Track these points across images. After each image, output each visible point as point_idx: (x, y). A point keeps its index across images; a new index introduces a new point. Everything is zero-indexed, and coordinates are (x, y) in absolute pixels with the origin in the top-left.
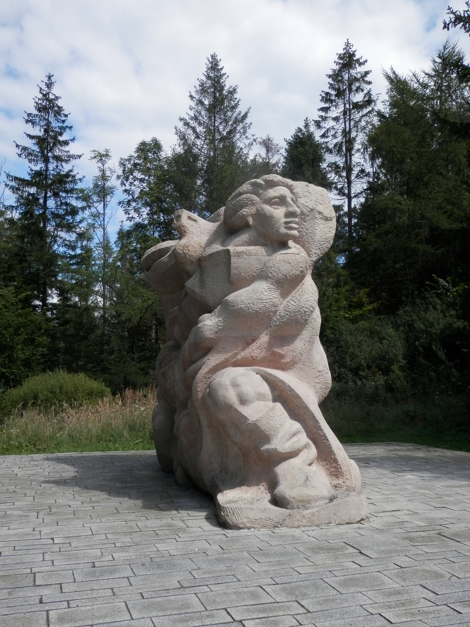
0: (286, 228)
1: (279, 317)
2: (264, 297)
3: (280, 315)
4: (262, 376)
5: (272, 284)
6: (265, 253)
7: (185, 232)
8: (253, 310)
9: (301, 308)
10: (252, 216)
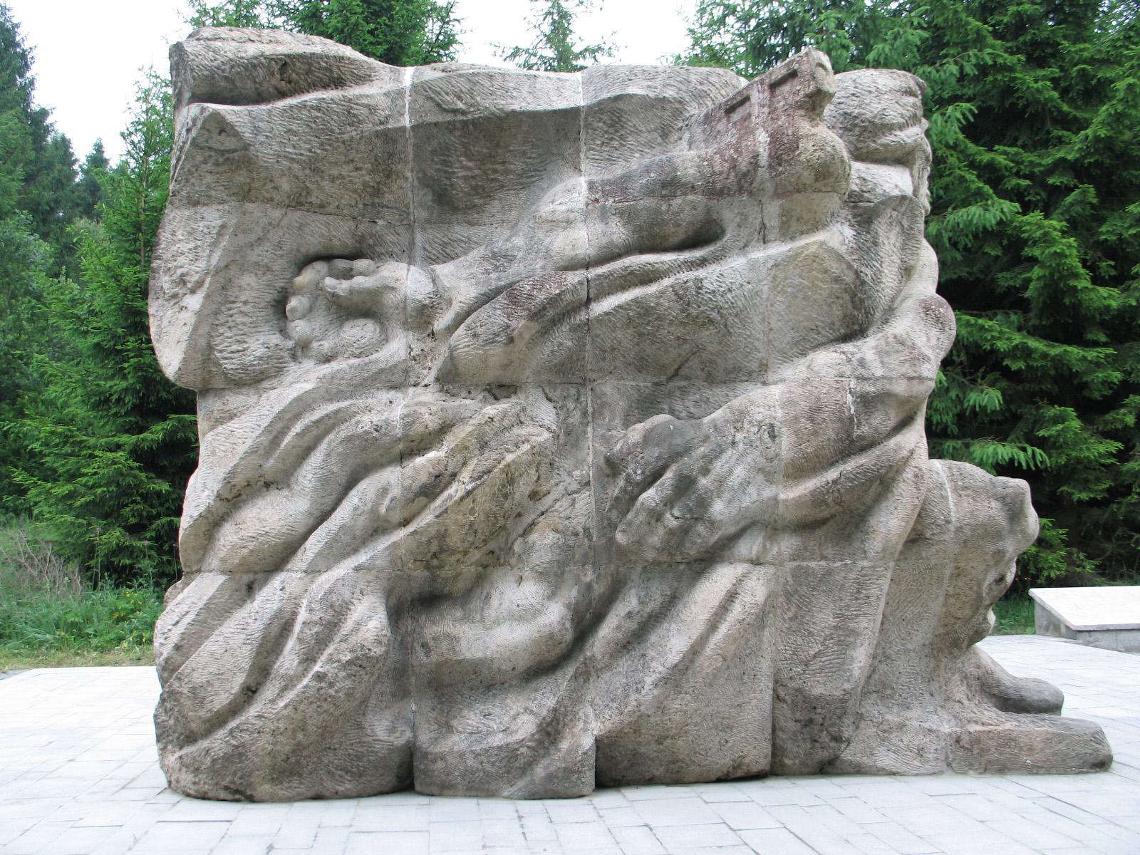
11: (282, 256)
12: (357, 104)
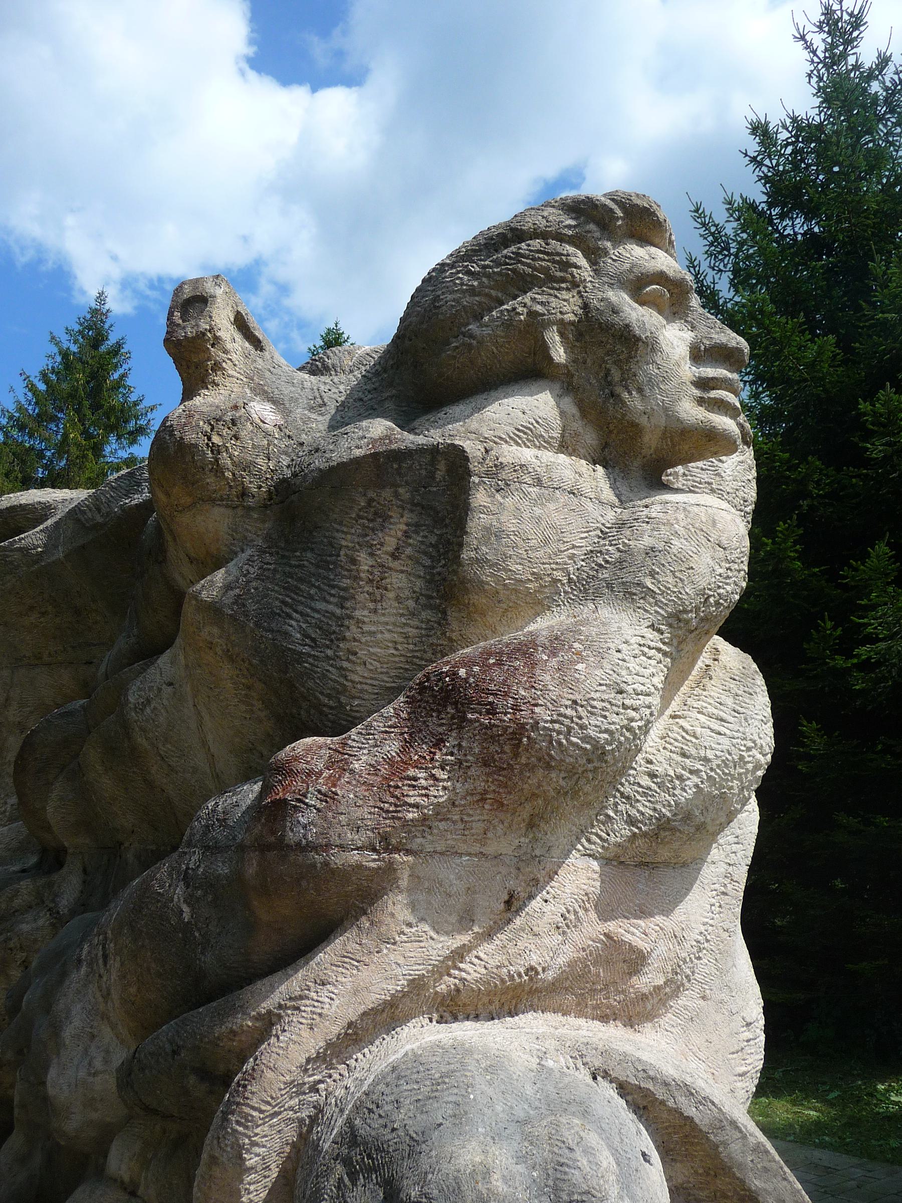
0: (701, 401)
1: (645, 781)
2: (629, 679)
3: (652, 775)
4: (623, 1089)
5: (652, 626)
6: (608, 494)
7: (217, 367)
8: (586, 739)
9: (749, 749)
10: (563, 327)
11: (31, 712)
12: (12, 551)
